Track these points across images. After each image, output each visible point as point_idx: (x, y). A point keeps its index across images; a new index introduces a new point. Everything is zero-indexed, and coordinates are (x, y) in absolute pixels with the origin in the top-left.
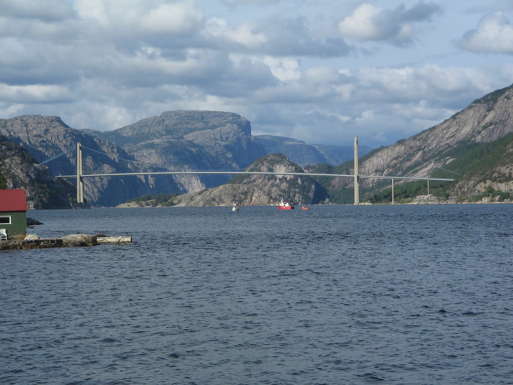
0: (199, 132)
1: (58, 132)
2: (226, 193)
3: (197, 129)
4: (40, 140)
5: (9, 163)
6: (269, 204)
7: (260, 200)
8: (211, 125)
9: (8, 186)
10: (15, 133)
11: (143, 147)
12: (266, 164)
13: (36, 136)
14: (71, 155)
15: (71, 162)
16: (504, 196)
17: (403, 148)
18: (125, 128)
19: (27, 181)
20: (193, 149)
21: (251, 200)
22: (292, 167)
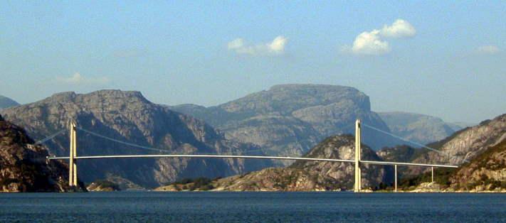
4: (115, 116)
8: (324, 100)
10: (87, 109)
13: (111, 112)
14: (149, 133)
15: (149, 141)
16: (497, 184)
17: (487, 129)
18: (230, 102)
19: (13, 162)
20: (299, 128)
21: (295, 185)
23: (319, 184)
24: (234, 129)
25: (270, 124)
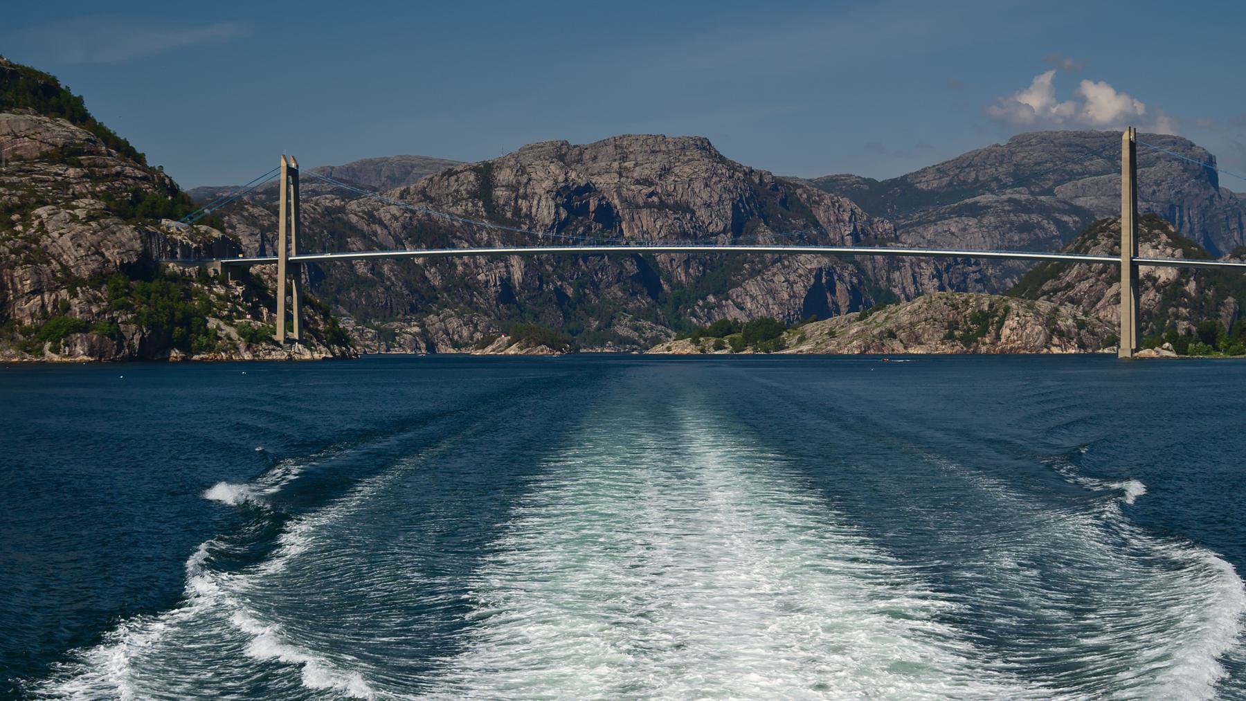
0: (1090, 179)
1: (691, 172)
2: (929, 316)
3: (1087, 173)
4: (646, 190)
5: (45, 216)
6: (1049, 349)
7: (1021, 336)
9: (19, 287)
11: (950, 213)
12: (1103, 243)
13: (638, 182)
18: (924, 170)
20: (1065, 218)
21: (998, 337)
22: (1173, 251)
23: (1061, 334)
24: (930, 222)
25: (1004, 211)
